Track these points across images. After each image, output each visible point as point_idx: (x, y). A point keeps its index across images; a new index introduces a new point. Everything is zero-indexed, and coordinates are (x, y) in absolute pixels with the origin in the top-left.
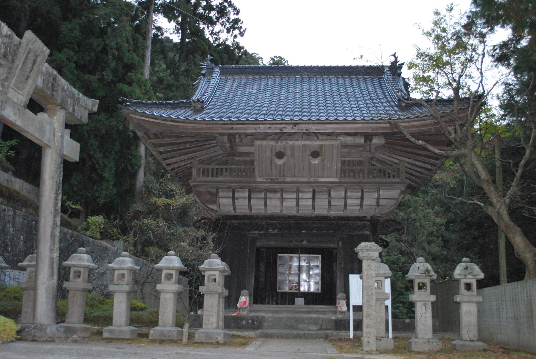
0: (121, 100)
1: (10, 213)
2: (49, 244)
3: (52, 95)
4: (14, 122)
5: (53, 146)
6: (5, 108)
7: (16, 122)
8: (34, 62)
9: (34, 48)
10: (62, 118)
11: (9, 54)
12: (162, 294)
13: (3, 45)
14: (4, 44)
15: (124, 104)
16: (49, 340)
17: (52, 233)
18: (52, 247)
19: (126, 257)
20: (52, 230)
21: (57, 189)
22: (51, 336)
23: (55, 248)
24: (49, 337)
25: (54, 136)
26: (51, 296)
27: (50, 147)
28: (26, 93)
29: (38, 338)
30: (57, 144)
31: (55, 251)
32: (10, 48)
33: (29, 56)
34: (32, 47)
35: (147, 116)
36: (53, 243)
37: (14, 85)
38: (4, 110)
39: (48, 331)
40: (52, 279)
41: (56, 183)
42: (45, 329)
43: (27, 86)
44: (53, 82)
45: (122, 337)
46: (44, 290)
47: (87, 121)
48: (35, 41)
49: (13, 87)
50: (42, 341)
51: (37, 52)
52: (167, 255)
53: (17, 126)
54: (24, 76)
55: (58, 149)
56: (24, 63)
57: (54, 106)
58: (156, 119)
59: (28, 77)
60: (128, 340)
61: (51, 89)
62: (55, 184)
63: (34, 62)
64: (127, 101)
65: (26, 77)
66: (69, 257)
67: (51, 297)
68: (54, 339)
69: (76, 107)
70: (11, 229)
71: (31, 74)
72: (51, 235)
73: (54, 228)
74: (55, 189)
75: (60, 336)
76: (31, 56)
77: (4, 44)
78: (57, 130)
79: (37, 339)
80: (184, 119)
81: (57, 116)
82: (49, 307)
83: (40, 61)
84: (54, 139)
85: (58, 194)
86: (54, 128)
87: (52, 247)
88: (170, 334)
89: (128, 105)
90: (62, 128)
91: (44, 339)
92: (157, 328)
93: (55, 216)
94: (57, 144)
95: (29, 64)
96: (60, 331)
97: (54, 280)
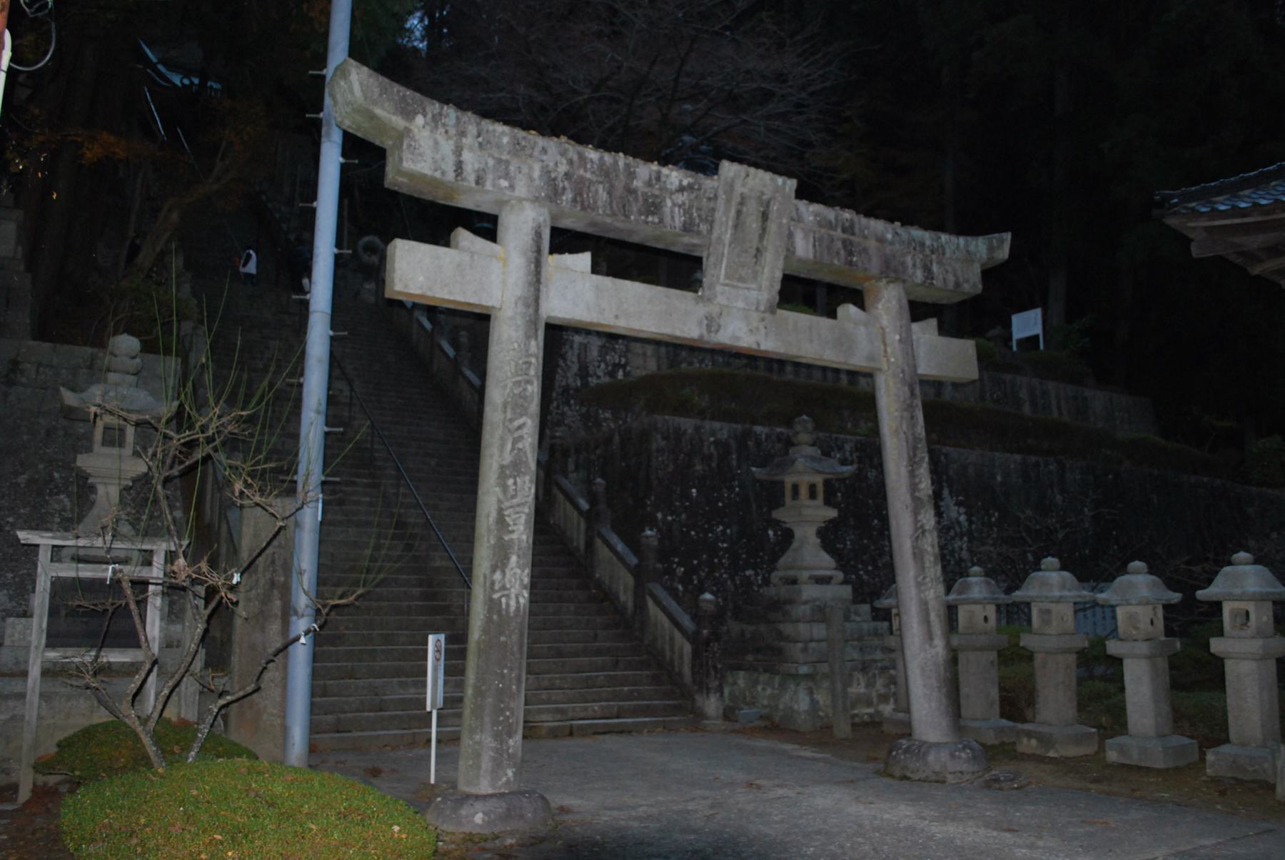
0: (1158, 197)
1: (1051, 467)
2: (912, 573)
3: (851, 263)
4: (755, 346)
5: (885, 367)
6: (719, 326)
7: (758, 344)
8: (765, 216)
9: (751, 190)
10: (894, 302)
11: (697, 221)
12: (1226, 661)
13: (676, 209)
14: (680, 206)
15: (1167, 205)
16: (934, 778)
17: (914, 548)
18: (920, 579)
19: (1139, 573)
20: (912, 542)
21: (911, 454)
22: (937, 768)
23: (928, 580)
24: (934, 772)
25: (885, 345)
26: (934, 682)
27: (880, 370)
28: (765, 283)
29: (912, 772)
30: (893, 360)
31: (930, 585)
32: (699, 209)
33: (745, 209)
34: (745, 191)
35: (1224, 214)
36: (922, 568)
37: (727, 276)
38: (717, 331)
39: (931, 758)
40: (930, 646)
41: (907, 442)
42: (924, 755)
43: (763, 269)
44: (845, 236)
45: (1148, 764)
46: (917, 671)
47: (980, 287)
48: (748, 175)
49: (727, 282)
50: (919, 780)
51: (763, 193)
52: (1230, 563)
53: (766, 352)
54: (746, 251)
55: (899, 370)
56: (736, 226)
57: (873, 281)
58: (1244, 216)
59: (758, 250)
60: (1159, 771)
61: (842, 252)
62: (904, 444)
63: (765, 216)
64: (1173, 197)
65: (753, 252)
66: (1023, 580)
67: (935, 684)
68: (945, 777)
69: (935, 268)
70: (1059, 497)
71: (765, 242)
72: (914, 554)
73: (917, 538)
74: (906, 456)
75: (958, 769)
76: (752, 209)
77: (680, 206)
78: (887, 330)
79: (909, 774)
80: (1271, 204)
81: (883, 300)
82: (933, 705)
83: (778, 209)
84: (885, 351)
85: (915, 463)
86: (882, 328)
87: (920, 579)
88: (1257, 767)
89: (1176, 205)
90: (898, 324)
91: (923, 776)
92: (1225, 749)
93: (916, 513)
94: (893, 360)
95: (753, 224)
96: (960, 758)
97: (936, 647)
